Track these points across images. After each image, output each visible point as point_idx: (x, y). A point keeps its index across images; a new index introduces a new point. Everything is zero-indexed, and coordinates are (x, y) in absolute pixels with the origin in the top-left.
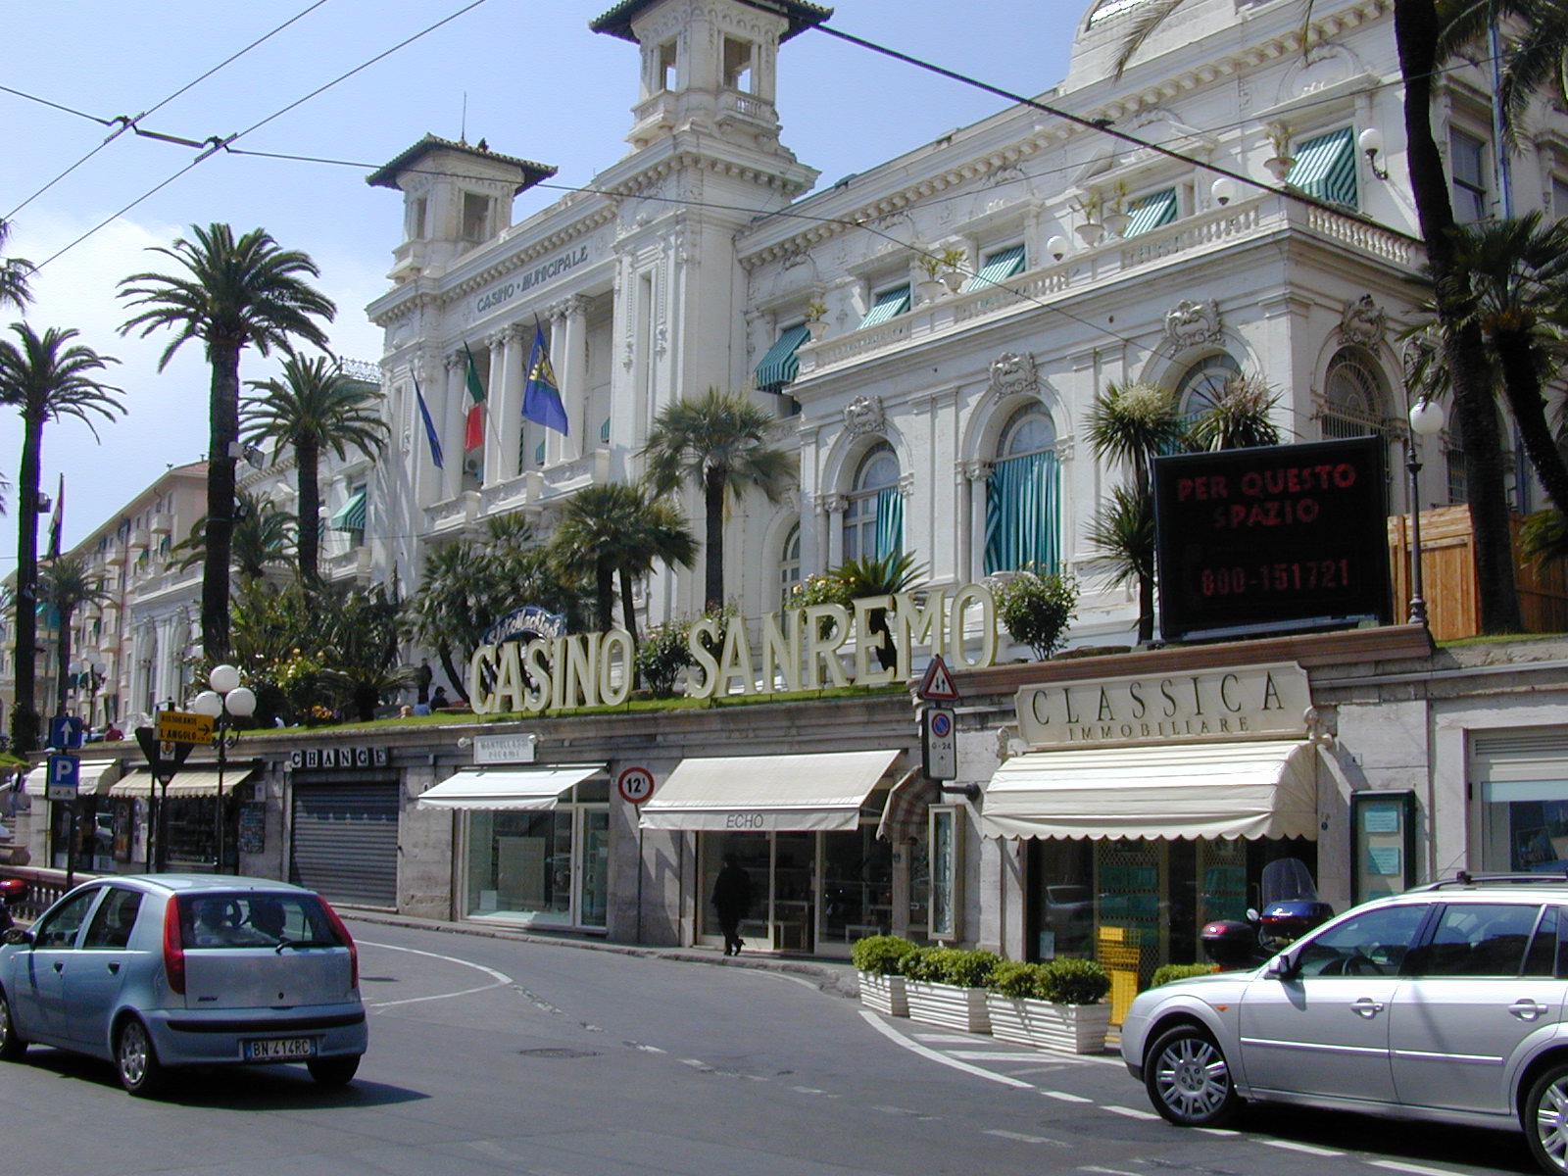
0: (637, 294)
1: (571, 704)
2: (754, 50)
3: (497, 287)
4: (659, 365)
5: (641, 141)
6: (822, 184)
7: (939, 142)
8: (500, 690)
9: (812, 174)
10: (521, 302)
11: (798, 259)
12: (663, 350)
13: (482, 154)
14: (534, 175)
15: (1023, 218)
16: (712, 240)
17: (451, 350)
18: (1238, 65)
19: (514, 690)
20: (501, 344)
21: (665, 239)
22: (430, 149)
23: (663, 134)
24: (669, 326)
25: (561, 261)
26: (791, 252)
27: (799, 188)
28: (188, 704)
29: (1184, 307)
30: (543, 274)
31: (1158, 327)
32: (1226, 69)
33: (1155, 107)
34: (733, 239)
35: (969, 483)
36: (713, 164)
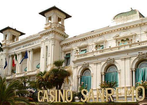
0: (45, 48)
1: (59, 101)
2: (62, 19)
3: (19, 46)
4: (49, 58)
5: (46, 28)
6: (69, 37)
7: (92, 32)
8: (44, 98)
9: (68, 36)
10: (22, 49)
11: (68, 46)
12: (49, 56)
13: (15, 30)
14: (22, 34)
15: (103, 42)
16: (57, 42)
17: (10, 55)
18: (140, 25)
19: (47, 98)
20: (19, 54)
21: (50, 41)
22: (8, 28)
23: (50, 28)
24: (51, 53)
25: (29, 44)
26: (67, 45)
27: (66, 37)
28: (65, 85)
29: (109, 58)
30: (26, 46)
31: (136, 55)
32: (138, 25)
33: (126, 29)
34: (60, 43)
35: (102, 75)
36: (57, 32)
